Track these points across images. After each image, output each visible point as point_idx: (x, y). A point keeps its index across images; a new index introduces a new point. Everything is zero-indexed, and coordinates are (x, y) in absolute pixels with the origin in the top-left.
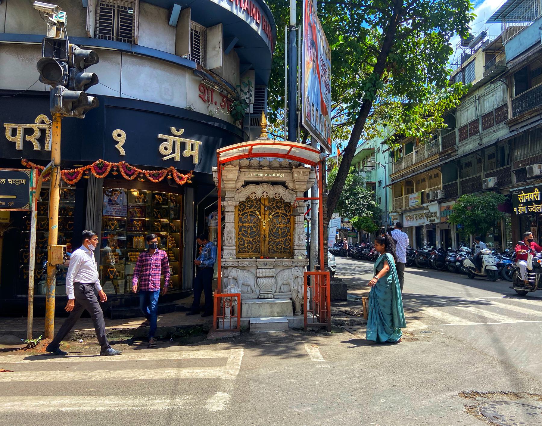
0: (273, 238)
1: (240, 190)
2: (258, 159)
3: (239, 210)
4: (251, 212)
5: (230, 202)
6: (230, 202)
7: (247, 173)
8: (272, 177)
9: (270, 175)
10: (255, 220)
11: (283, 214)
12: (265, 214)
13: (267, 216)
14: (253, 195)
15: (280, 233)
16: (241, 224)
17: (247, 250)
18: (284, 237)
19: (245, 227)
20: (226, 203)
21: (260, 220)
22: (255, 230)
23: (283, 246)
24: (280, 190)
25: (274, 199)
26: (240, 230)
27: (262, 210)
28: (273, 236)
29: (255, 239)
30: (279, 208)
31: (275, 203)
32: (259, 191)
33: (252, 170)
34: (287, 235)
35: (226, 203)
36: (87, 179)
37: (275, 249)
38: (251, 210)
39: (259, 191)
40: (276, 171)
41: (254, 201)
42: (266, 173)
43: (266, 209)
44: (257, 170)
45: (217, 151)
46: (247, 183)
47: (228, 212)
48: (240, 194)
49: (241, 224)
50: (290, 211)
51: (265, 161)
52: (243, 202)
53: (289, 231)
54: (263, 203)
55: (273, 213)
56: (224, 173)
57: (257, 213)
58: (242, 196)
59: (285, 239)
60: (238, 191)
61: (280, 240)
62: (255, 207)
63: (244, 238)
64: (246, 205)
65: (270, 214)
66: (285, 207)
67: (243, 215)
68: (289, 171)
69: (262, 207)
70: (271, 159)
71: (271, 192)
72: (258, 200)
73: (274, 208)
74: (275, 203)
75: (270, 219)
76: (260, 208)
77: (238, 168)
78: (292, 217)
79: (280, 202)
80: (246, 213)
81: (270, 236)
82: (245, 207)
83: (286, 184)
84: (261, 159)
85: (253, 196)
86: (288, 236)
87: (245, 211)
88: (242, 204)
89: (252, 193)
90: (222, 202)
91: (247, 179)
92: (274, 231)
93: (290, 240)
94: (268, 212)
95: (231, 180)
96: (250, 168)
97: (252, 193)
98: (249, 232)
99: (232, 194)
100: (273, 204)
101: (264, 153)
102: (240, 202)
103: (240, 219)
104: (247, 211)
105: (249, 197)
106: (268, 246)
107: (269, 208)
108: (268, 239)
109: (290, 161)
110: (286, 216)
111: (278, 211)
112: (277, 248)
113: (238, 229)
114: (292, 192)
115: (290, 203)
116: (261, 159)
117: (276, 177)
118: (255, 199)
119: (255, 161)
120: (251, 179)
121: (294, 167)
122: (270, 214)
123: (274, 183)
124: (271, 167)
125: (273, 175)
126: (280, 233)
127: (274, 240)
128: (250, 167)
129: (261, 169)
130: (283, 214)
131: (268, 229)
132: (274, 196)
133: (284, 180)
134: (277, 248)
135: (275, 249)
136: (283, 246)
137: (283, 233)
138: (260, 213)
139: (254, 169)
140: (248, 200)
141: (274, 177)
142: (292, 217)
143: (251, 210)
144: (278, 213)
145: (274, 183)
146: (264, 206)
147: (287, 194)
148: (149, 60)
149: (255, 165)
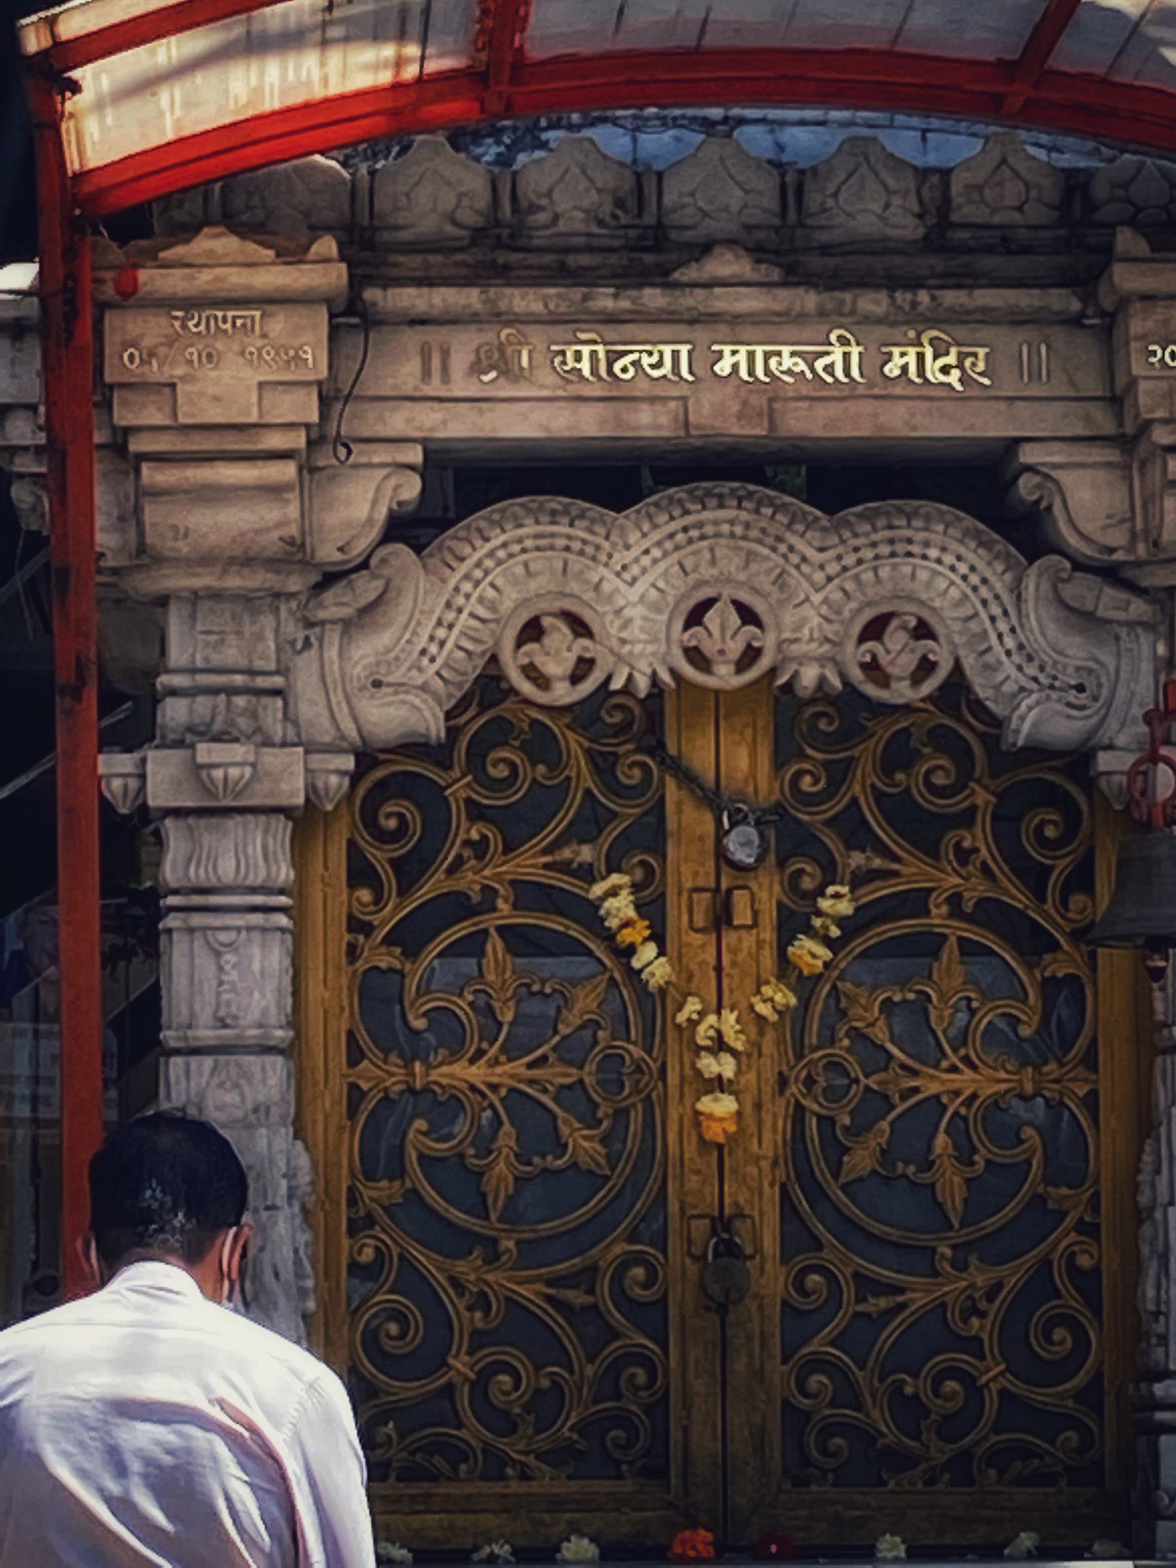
0: (833, 1253)
1: (367, 588)
2: (612, 140)
3: (360, 872)
4: (529, 894)
5: (228, 760)
6: (228, 760)
7: (463, 346)
8: (817, 391)
9: (788, 361)
10: (586, 1002)
11: (990, 913)
12: (722, 918)
13: (751, 944)
14: (557, 654)
15: (951, 1183)
16: (384, 1075)
17: (473, 1432)
18: (993, 1248)
19: (443, 1107)
20: (163, 777)
21: (653, 1005)
22: (583, 1143)
23: (993, 1373)
24: (944, 570)
25: (849, 710)
26: (379, 1156)
27: (687, 868)
28: (852, 1233)
29: (587, 1278)
30: (925, 831)
31: (866, 754)
32: (636, 597)
33: (524, 300)
34: (1042, 1216)
35: (163, 777)
36: (151, 888)
37: (879, 1418)
38: (528, 864)
39: (636, 597)
40: (873, 302)
41: (574, 744)
42: (737, 327)
43: (742, 845)
44: (605, 300)
45: (33, 42)
46: (466, 486)
47: (204, 897)
48: (367, 650)
49: (384, 1075)
50: (1081, 879)
51: (708, 165)
52: (414, 747)
53: (1068, 1161)
54: (700, 755)
55: (838, 903)
56: (135, 342)
57: (621, 907)
58: (396, 667)
59: (1014, 1274)
60: (336, 605)
61: (953, 1287)
62: (579, 832)
63: (1017, 898)
64: (459, 788)
65: (793, 922)
66: (1005, 822)
67: (409, 937)
68: (1062, 300)
69: (688, 820)
70: (807, 133)
71: (814, 599)
72: (633, 724)
73: (854, 830)
74: (866, 754)
75: (805, 985)
76: (651, 835)
77: (335, 276)
78: (1114, 962)
79: (941, 739)
80: (457, 907)
81: (797, 1238)
82: (438, 826)
83: (1026, 486)
84: (657, 143)
85: (557, 666)
86: (1064, 1239)
87: (426, 891)
88: (388, 775)
89: (533, 631)
90: (115, 766)
91: (460, 426)
92: (861, 1159)
93: (1087, 1282)
94: (764, 895)
95: (234, 441)
96: (503, 274)
97: (533, 631)
98: (502, 1170)
99: (257, 643)
100: (838, 775)
101: (695, 56)
102: (367, 757)
103: (377, 996)
104: (470, 882)
105: (489, 685)
106: (777, 1370)
107: (787, 837)
108: (771, 1279)
109: (1074, 155)
110: (1034, 943)
111: (914, 871)
112: (909, 1411)
113: (349, 1147)
114: (1109, 601)
115: (1078, 760)
116: (657, 143)
117: (879, 388)
118: (583, 715)
119: (569, 173)
120: (525, 417)
121: (1126, 240)
122: (793, 922)
123: (845, 480)
124: (806, 257)
125: (840, 358)
126: (951, 1183)
127: (866, 1285)
128: (498, 249)
129: (661, 277)
130: (990, 913)
131: (770, 1140)
132: (853, 655)
133: (990, 424)
134: (909, 1411)
135: (879, 1418)
136: (993, 1373)
137: (985, 1191)
138: (652, 908)
139: (562, 275)
140: (474, 723)
141: (848, 393)
142: (1114, 962)
143: (528, 864)
144: (916, 902)
145: (845, 480)
146: (712, 798)
147: (1042, 626)
148: (233, 295)
149: (574, 222)
